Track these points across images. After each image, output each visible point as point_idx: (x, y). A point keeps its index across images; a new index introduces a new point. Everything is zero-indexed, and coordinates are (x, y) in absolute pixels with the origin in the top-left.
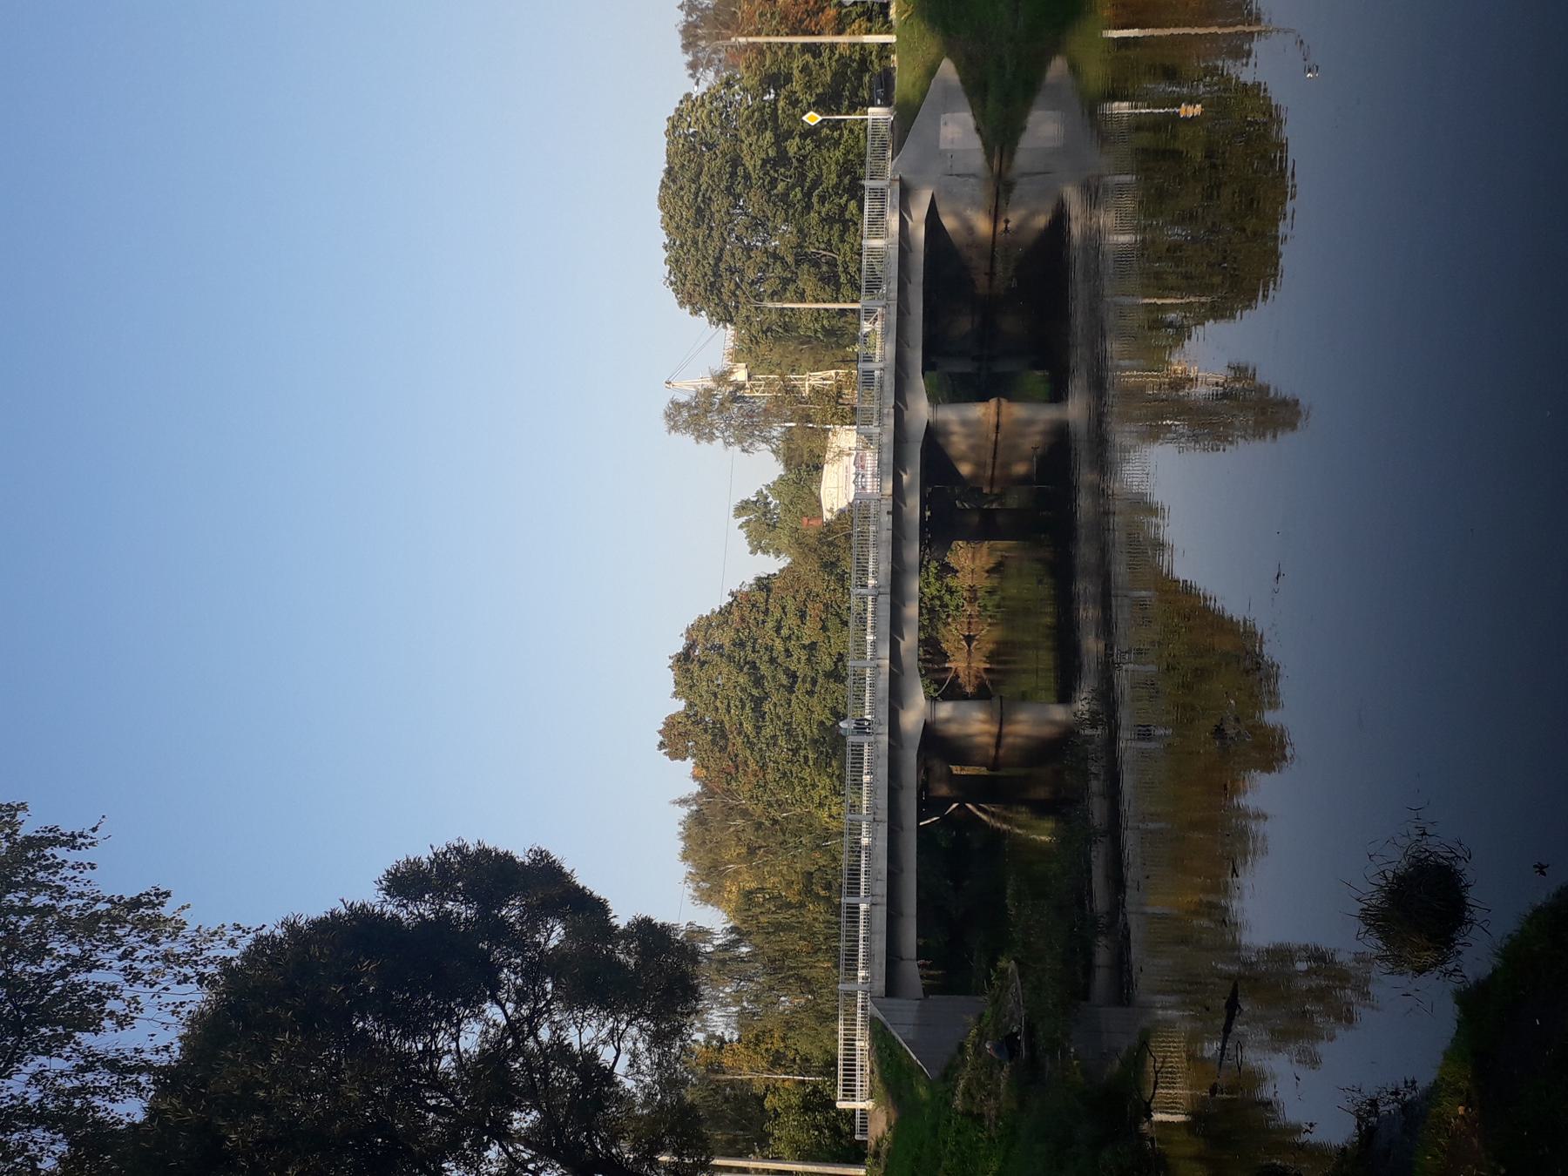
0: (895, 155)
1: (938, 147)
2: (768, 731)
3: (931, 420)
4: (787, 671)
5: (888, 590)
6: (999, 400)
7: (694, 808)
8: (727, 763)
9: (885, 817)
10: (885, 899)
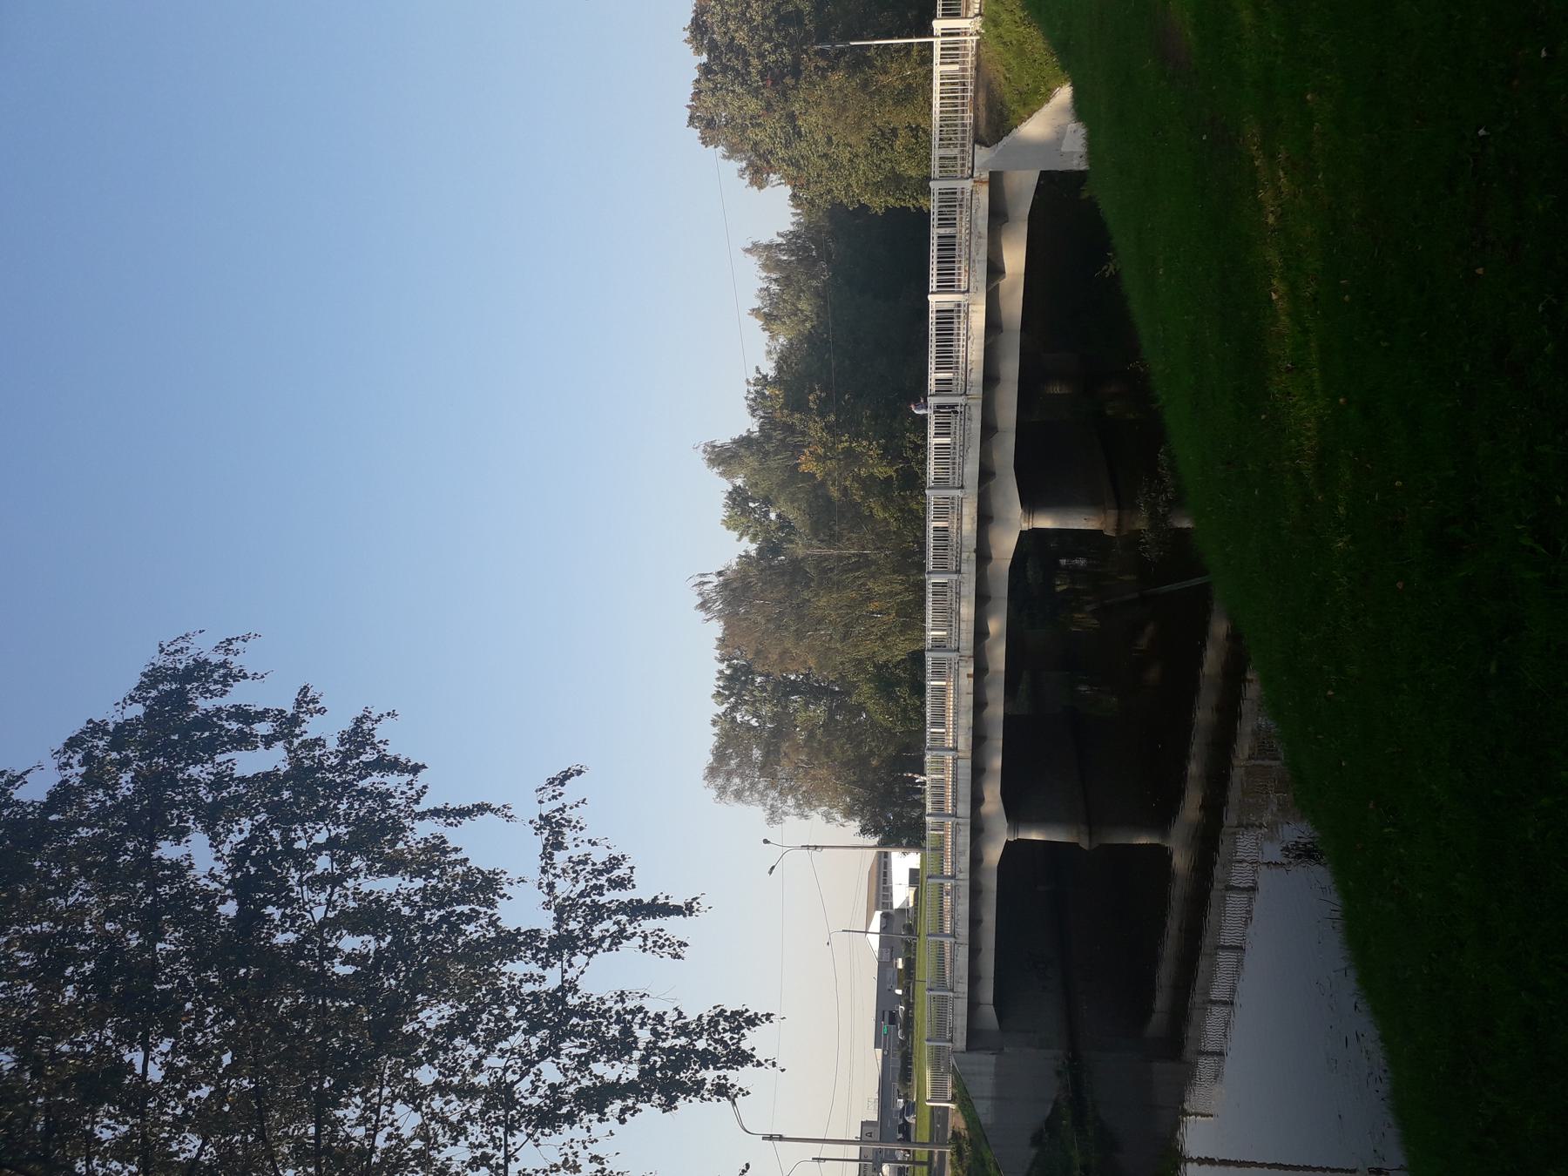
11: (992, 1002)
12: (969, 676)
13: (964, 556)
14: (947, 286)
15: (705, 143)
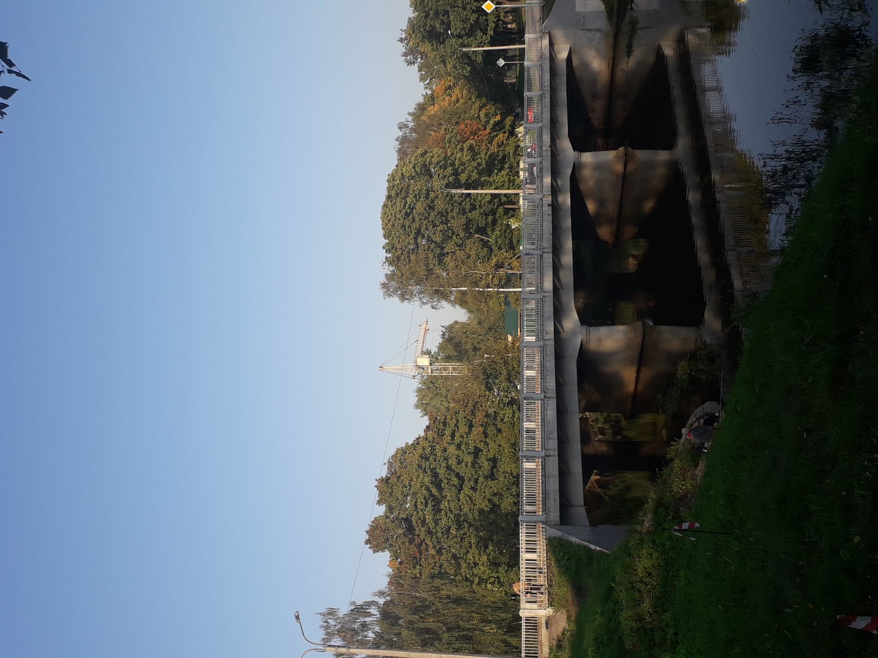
0: (545, 18)
1: (575, 10)
2: (443, 522)
3: (576, 162)
4: (458, 475)
5: (551, 250)
6: (625, 148)
7: (388, 598)
8: (413, 549)
9: (554, 394)
10: (557, 453)
11: (583, 504)
12: (548, 205)
13: (544, 149)
14: (529, 90)
15: (384, 248)
